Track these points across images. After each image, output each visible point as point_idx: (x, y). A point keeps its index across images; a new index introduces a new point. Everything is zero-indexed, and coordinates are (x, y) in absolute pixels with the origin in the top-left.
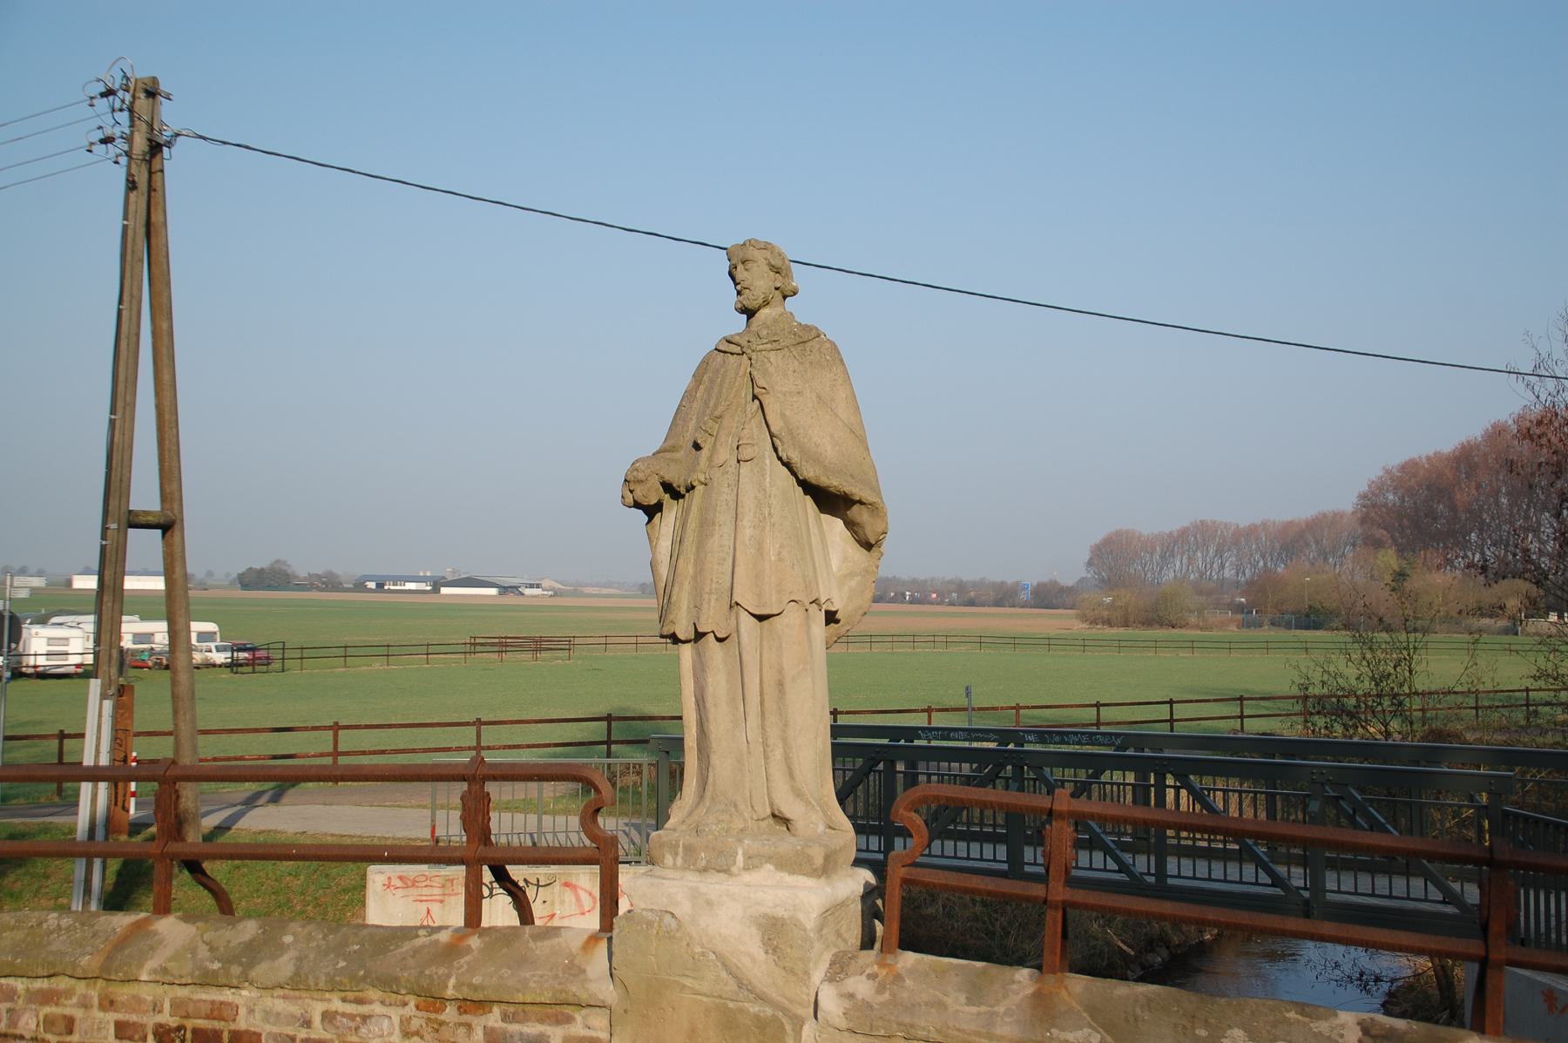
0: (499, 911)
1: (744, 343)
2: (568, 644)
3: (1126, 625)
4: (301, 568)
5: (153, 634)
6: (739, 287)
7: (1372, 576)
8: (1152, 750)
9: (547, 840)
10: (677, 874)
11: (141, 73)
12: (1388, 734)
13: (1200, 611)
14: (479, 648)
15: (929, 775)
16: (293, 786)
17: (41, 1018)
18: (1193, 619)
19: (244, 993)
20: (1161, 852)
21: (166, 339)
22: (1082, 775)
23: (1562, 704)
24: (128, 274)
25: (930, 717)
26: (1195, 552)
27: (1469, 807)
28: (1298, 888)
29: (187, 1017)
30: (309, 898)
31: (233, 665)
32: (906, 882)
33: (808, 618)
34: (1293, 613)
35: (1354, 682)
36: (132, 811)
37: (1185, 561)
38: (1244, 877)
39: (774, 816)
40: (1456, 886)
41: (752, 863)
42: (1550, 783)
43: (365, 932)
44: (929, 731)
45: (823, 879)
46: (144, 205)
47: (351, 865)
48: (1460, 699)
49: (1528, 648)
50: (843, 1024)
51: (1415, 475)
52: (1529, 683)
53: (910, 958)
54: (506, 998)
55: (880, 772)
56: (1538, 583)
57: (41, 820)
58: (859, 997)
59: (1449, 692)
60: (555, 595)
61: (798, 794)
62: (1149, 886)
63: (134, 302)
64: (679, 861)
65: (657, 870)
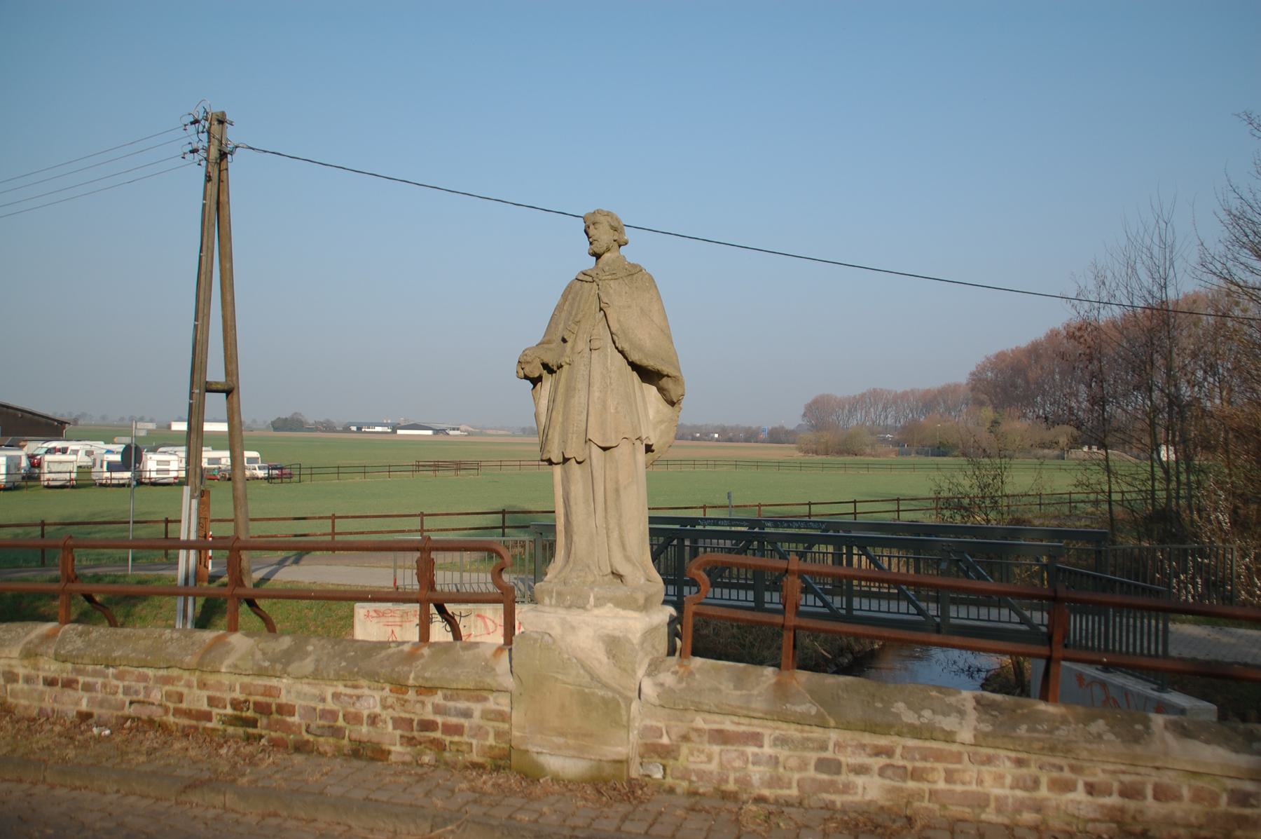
0: (439, 632)
1: (594, 274)
2: (477, 466)
3: (827, 454)
4: (311, 417)
5: (220, 459)
6: (591, 240)
7: (978, 423)
8: (844, 531)
9: (467, 588)
10: (552, 610)
11: (216, 109)
12: (988, 521)
13: (873, 445)
14: (421, 468)
15: (705, 548)
16: (307, 553)
17: (164, 693)
18: (868, 450)
19: (284, 681)
20: (850, 595)
21: (228, 274)
22: (801, 548)
23: (1091, 501)
24: (206, 234)
25: (705, 511)
26: (869, 408)
27: (1036, 565)
28: (933, 616)
29: (250, 694)
30: (319, 623)
31: (269, 478)
32: (696, 614)
33: (634, 449)
34: (930, 446)
35: (968, 489)
36: (210, 568)
37: (863, 414)
38: (900, 609)
39: (613, 573)
40: (1028, 613)
41: (600, 602)
42: (1082, 550)
43: (356, 645)
44: (705, 520)
45: (644, 613)
46: (216, 191)
47: (344, 603)
48: (1031, 499)
49: (1072, 467)
50: (657, 702)
51: (1004, 361)
52: (1072, 489)
53: (698, 661)
54: (446, 686)
55: (675, 546)
56: (1078, 428)
57: (155, 573)
58: (667, 685)
59: (1026, 495)
60: (469, 435)
61: (628, 559)
62: (842, 615)
63: (209, 251)
64: (554, 602)
65: (539, 606)
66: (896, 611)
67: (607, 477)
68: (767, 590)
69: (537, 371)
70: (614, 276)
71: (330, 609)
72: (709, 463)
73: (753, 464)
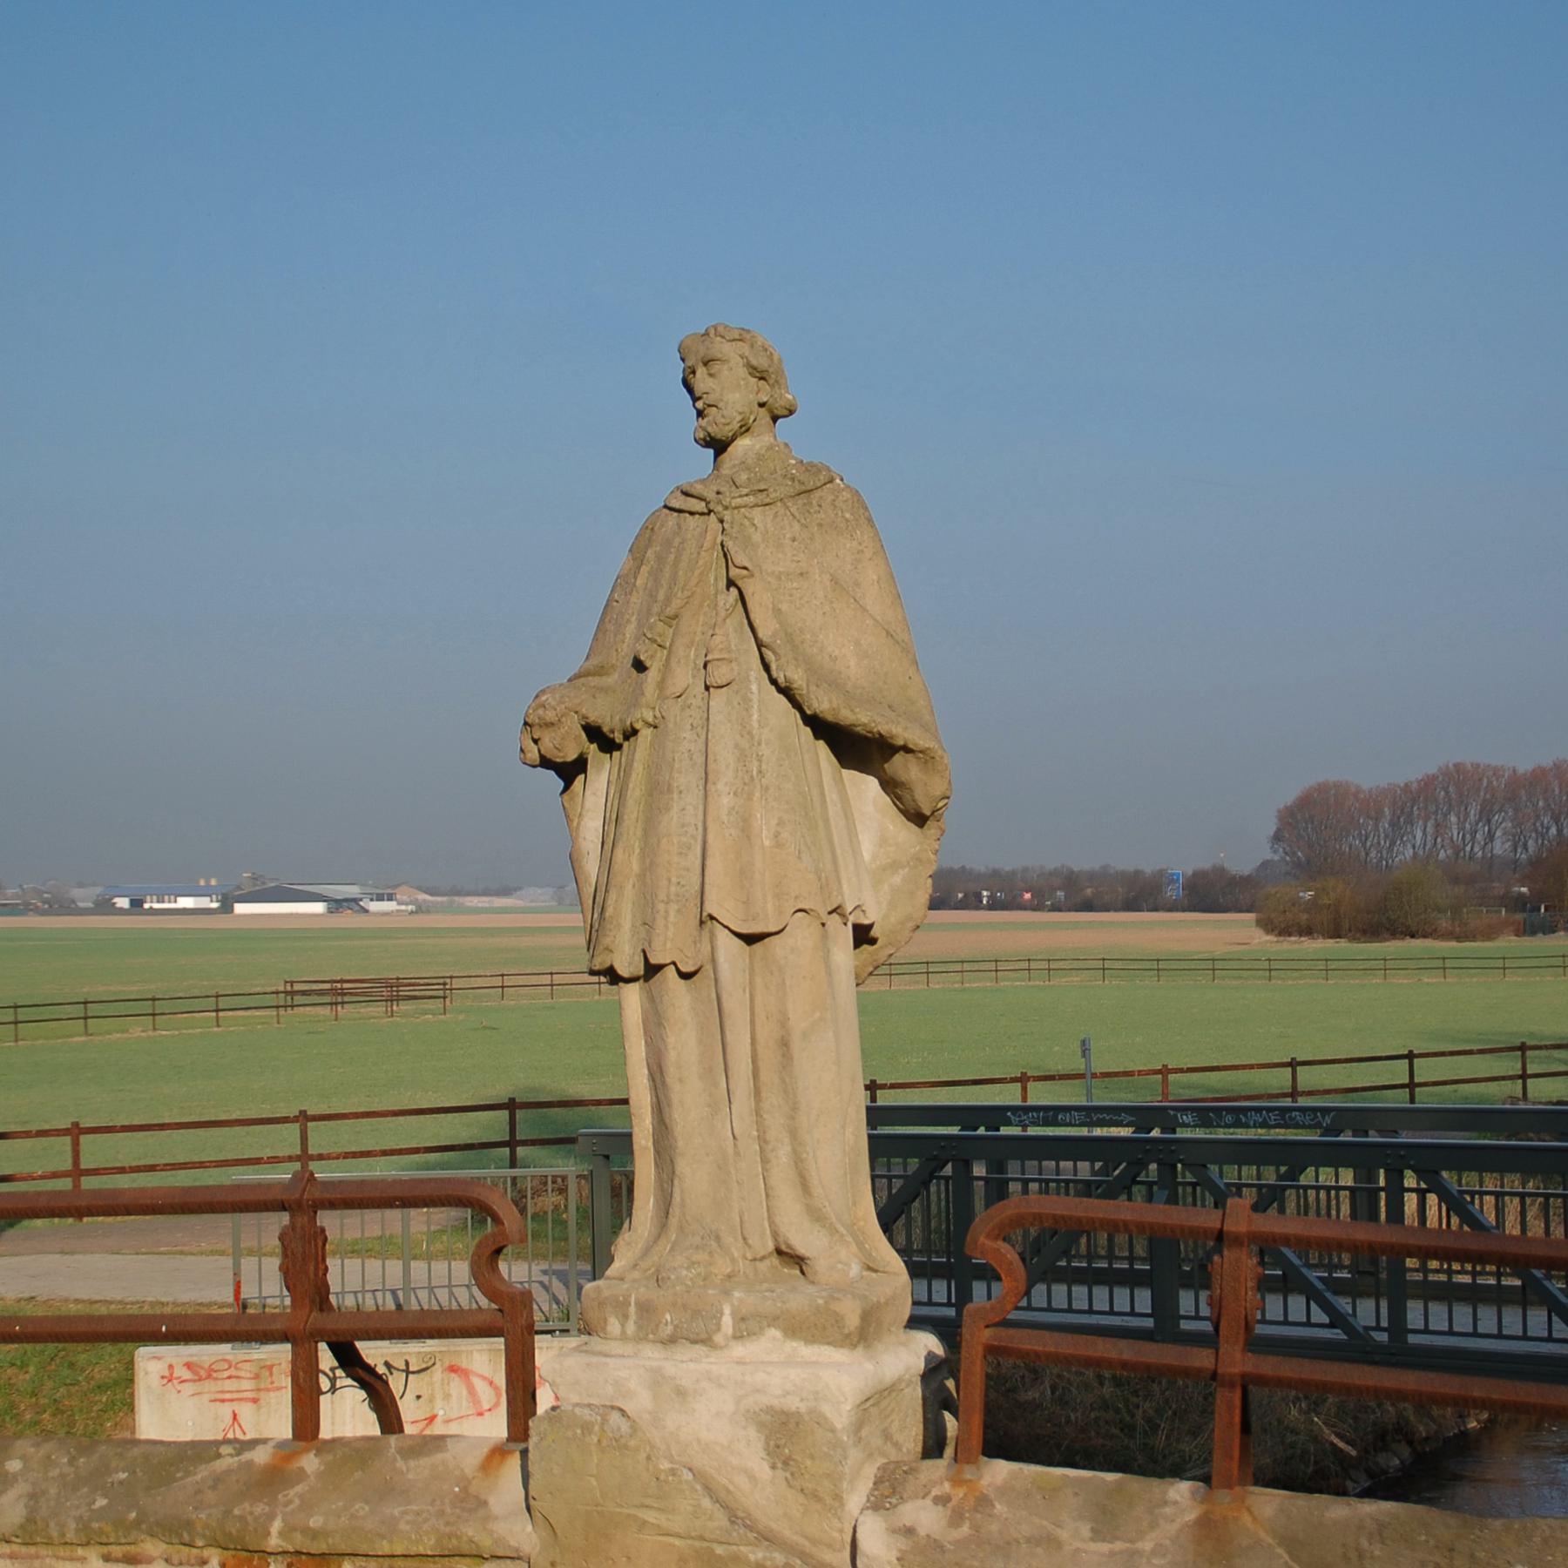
1: (711, 495)
2: (442, 989)
3: (1336, 934)
6: (700, 405)
8: (1381, 1132)
9: (420, 1300)
10: (628, 1349)
14: (298, 999)
15: (1025, 1182)
16: (11, 1225)
18: (1444, 923)
20: (1398, 1293)
22: (1270, 1176)
25: (1024, 1089)
26: (1445, 815)
30: (44, 1401)
37: (1430, 829)
39: (779, 1252)
41: (747, 1327)
44: (1023, 1112)
47: (108, 1347)
53: (1000, 1471)
54: (364, 1549)
55: (947, 1179)
61: (816, 1215)
64: (631, 1328)
65: (595, 1342)
66: (1045, 1305)
67: (757, 1010)
68: (1187, 1286)
69: (571, 745)
70: (761, 497)
71: (72, 1365)
72: (1033, 965)
73: (1148, 965)
